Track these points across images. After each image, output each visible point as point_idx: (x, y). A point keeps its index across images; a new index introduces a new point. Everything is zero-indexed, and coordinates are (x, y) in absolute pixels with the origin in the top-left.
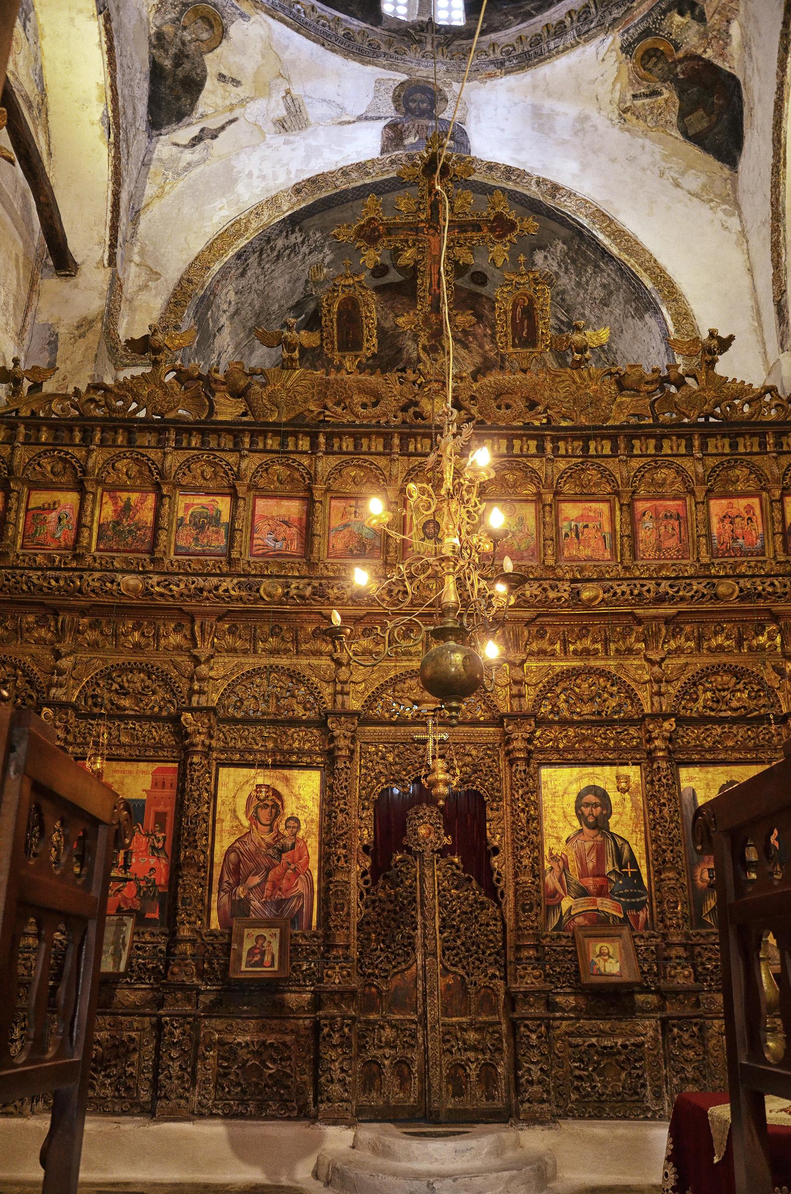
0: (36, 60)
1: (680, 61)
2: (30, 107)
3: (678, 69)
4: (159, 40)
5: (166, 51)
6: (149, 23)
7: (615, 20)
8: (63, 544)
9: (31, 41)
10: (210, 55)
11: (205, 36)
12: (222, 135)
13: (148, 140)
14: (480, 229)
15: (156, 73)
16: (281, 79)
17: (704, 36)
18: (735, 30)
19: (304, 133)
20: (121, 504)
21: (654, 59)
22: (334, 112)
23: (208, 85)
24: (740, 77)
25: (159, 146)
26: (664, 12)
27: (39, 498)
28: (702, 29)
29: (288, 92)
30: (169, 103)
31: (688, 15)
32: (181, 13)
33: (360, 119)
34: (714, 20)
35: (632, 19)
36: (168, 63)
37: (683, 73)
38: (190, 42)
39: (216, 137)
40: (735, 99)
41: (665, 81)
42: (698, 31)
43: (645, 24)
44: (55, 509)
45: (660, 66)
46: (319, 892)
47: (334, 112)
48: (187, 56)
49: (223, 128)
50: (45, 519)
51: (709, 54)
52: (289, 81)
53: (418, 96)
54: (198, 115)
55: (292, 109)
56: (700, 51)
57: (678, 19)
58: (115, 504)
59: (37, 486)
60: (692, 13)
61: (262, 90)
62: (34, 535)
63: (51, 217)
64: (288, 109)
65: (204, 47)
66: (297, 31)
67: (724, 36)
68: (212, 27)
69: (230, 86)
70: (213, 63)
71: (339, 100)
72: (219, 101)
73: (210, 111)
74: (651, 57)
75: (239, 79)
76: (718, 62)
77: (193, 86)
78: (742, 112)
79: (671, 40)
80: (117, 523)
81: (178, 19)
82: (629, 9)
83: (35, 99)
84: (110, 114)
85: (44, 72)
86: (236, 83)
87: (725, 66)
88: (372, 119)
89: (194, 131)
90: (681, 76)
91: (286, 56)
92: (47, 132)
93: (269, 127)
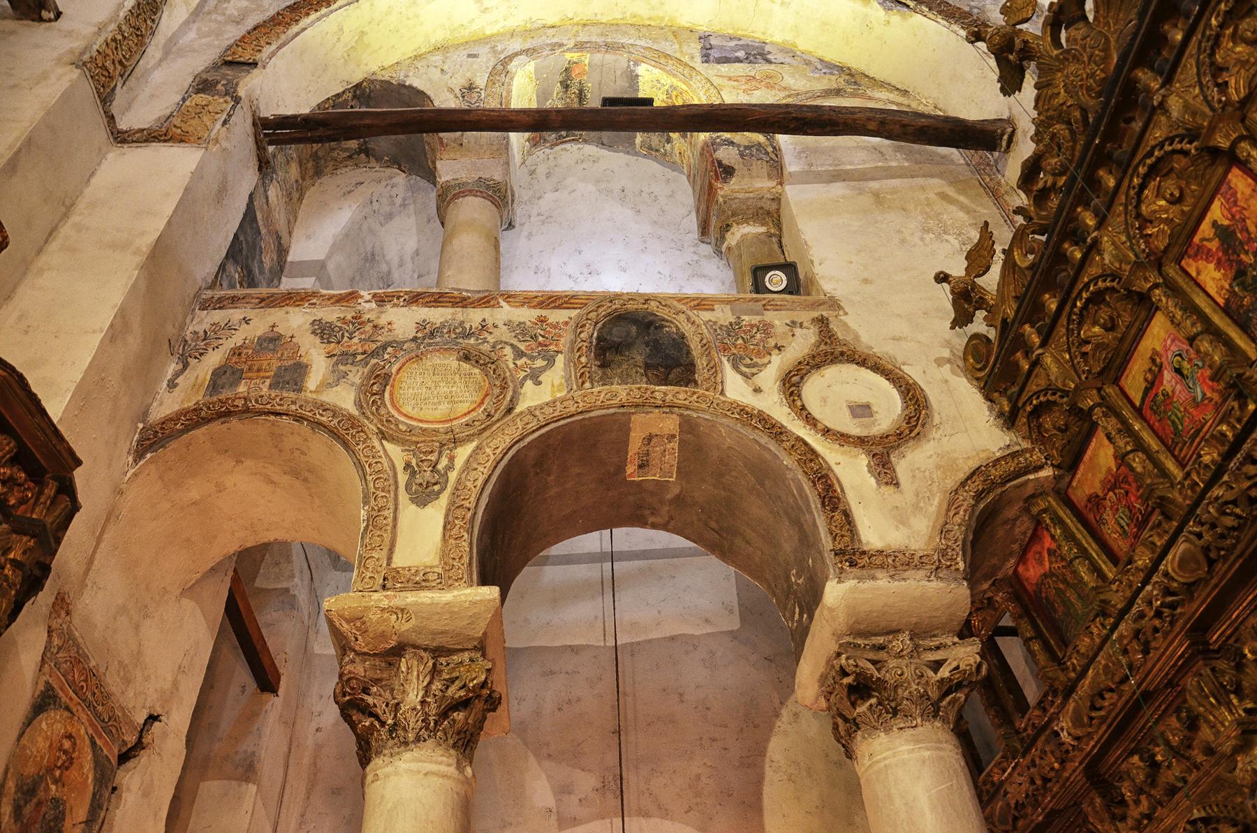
0: (808, 63)
2: (838, 92)
8: (1216, 397)
9: (788, 60)
20: (1214, 245)
27: (1134, 380)
44: (1160, 367)
46: (1153, 13)
50: (1166, 395)
58: (1208, 256)
59: (1115, 368)
62: (1177, 432)
63: (904, 126)
80: (1240, 274)
83: (833, 81)
85: (827, 59)
92: (883, 85)
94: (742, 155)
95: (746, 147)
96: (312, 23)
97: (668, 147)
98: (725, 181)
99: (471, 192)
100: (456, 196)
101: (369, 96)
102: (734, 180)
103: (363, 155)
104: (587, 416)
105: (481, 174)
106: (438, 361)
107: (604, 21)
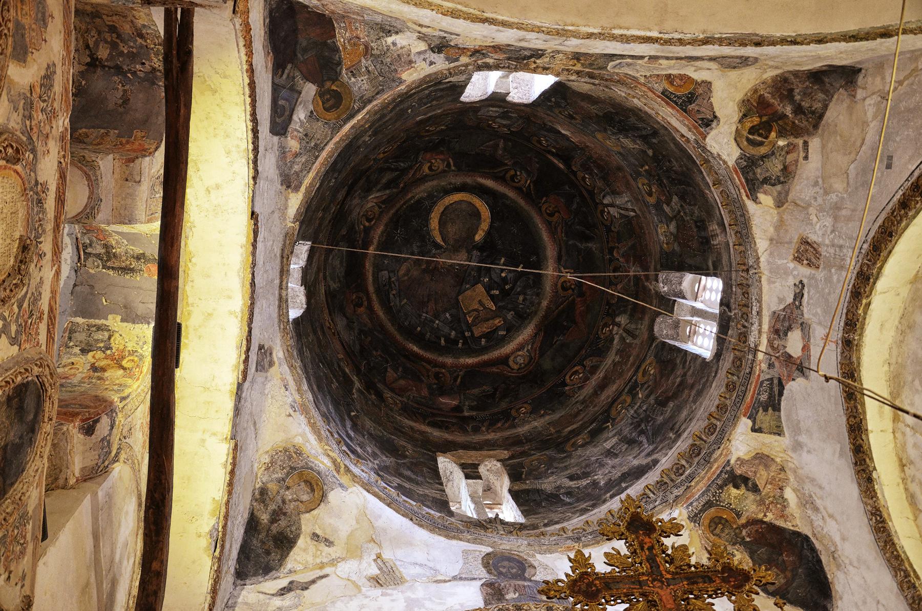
1: (744, 526)
3: (744, 533)
4: (262, 495)
5: (266, 506)
6: (256, 479)
7: (676, 497)
10: (307, 515)
11: (305, 497)
12: (313, 587)
13: (232, 587)
14: (711, 581)
15: (252, 525)
16: (372, 543)
17: (761, 502)
18: (789, 494)
19: (401, 588)
21: (720, 526)
22: (429, 573)
23: (301, 542)
24: (806, 530)
25: (244, 593)
26: (721, 487)
28: (758, 498)
29: (379, 556)
30: (258, 556)
31: (743, 487)
32: (288, 474)
33: (454, 578)
34: (767, 490)
35: (692, 496)
36: (265, 518)
37: (749, 536)
38: (290, 501)
39: (307, 588)
40: (807, 552)
41: (734, 544)
42: (755, 500)
43: (706, 498)
45: (727, 531)
47: (429, 573)
48: (285, 514)
49: (314, 582)
51: (770, 517)
52: (380, 546)
53: (506, 563)
54: (286, 571)
55: (385, 569)
56: (760, 516)
57: (734, 491)
60: (746, 485)
61: (354, 551)
64: (380, 569)
65: (302, 507)
66: (389, 505)
67: (781, 501)
68: (313, 490)
69: (322, 546)
70: (308, 523)
71: (431, 565)
72: (310, 559)
73: (299, 567)
74: (717, 524)
75: (331, 539)
76: (780, 523)
77: (285, 543)
78: (820, 561)
79: (732, 509)
81: (283, 480)
82: (688, 487)
84: (220, 529)
86: (329, 543)
87: (788, 526)
88: (466, 579)
89: (284, 583)
90: (748, 539)
91: (379, 524)
93: (362, 582)
94: (103, 440)
95: (109, 442)
96: (240, 57)
97: (77, 350)
98: (81, 428)
99: (92, 193)
100: (88, 178)
101: (154, 83)
102: (81, 436)
103: (89, 60)
104: (144, 499)
105: (104, 200)
106: (20, 215)
107: (186, 287)
